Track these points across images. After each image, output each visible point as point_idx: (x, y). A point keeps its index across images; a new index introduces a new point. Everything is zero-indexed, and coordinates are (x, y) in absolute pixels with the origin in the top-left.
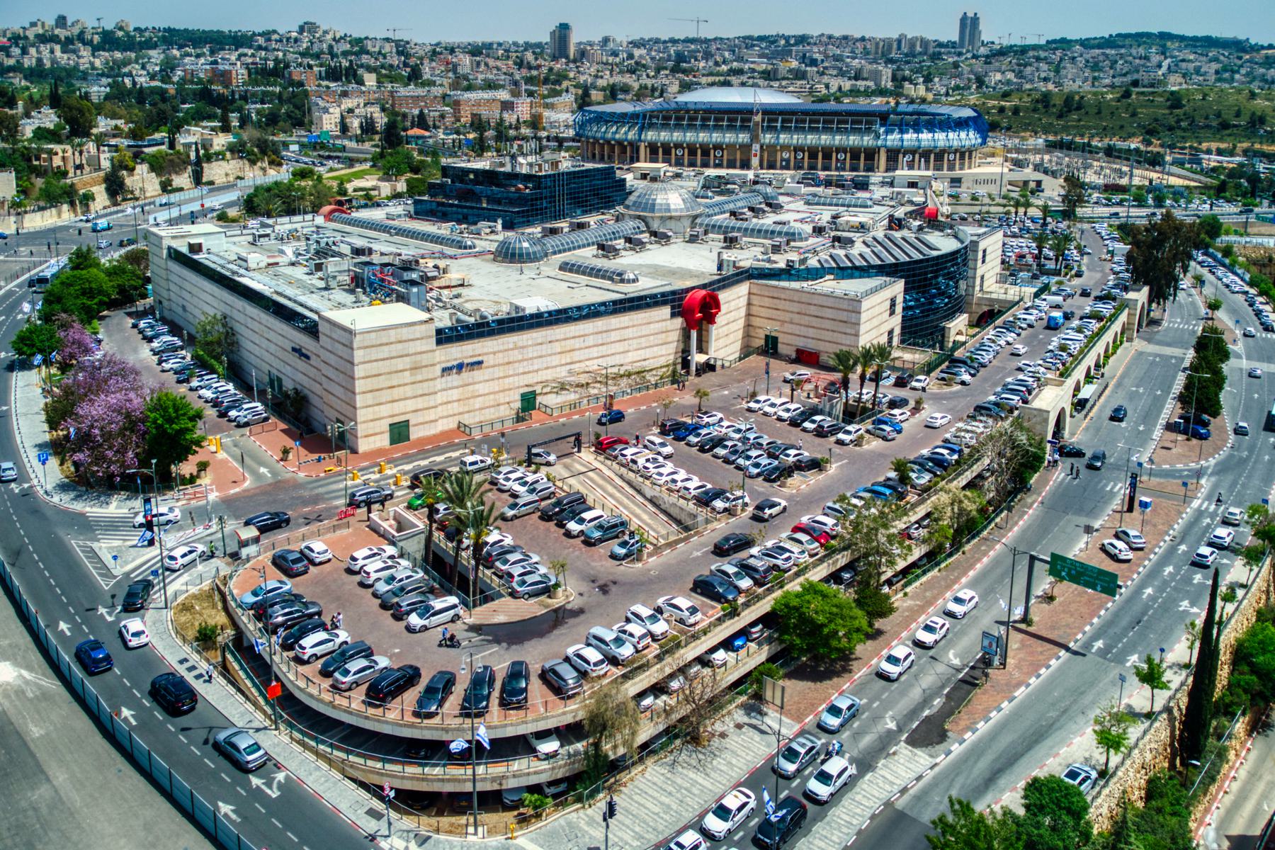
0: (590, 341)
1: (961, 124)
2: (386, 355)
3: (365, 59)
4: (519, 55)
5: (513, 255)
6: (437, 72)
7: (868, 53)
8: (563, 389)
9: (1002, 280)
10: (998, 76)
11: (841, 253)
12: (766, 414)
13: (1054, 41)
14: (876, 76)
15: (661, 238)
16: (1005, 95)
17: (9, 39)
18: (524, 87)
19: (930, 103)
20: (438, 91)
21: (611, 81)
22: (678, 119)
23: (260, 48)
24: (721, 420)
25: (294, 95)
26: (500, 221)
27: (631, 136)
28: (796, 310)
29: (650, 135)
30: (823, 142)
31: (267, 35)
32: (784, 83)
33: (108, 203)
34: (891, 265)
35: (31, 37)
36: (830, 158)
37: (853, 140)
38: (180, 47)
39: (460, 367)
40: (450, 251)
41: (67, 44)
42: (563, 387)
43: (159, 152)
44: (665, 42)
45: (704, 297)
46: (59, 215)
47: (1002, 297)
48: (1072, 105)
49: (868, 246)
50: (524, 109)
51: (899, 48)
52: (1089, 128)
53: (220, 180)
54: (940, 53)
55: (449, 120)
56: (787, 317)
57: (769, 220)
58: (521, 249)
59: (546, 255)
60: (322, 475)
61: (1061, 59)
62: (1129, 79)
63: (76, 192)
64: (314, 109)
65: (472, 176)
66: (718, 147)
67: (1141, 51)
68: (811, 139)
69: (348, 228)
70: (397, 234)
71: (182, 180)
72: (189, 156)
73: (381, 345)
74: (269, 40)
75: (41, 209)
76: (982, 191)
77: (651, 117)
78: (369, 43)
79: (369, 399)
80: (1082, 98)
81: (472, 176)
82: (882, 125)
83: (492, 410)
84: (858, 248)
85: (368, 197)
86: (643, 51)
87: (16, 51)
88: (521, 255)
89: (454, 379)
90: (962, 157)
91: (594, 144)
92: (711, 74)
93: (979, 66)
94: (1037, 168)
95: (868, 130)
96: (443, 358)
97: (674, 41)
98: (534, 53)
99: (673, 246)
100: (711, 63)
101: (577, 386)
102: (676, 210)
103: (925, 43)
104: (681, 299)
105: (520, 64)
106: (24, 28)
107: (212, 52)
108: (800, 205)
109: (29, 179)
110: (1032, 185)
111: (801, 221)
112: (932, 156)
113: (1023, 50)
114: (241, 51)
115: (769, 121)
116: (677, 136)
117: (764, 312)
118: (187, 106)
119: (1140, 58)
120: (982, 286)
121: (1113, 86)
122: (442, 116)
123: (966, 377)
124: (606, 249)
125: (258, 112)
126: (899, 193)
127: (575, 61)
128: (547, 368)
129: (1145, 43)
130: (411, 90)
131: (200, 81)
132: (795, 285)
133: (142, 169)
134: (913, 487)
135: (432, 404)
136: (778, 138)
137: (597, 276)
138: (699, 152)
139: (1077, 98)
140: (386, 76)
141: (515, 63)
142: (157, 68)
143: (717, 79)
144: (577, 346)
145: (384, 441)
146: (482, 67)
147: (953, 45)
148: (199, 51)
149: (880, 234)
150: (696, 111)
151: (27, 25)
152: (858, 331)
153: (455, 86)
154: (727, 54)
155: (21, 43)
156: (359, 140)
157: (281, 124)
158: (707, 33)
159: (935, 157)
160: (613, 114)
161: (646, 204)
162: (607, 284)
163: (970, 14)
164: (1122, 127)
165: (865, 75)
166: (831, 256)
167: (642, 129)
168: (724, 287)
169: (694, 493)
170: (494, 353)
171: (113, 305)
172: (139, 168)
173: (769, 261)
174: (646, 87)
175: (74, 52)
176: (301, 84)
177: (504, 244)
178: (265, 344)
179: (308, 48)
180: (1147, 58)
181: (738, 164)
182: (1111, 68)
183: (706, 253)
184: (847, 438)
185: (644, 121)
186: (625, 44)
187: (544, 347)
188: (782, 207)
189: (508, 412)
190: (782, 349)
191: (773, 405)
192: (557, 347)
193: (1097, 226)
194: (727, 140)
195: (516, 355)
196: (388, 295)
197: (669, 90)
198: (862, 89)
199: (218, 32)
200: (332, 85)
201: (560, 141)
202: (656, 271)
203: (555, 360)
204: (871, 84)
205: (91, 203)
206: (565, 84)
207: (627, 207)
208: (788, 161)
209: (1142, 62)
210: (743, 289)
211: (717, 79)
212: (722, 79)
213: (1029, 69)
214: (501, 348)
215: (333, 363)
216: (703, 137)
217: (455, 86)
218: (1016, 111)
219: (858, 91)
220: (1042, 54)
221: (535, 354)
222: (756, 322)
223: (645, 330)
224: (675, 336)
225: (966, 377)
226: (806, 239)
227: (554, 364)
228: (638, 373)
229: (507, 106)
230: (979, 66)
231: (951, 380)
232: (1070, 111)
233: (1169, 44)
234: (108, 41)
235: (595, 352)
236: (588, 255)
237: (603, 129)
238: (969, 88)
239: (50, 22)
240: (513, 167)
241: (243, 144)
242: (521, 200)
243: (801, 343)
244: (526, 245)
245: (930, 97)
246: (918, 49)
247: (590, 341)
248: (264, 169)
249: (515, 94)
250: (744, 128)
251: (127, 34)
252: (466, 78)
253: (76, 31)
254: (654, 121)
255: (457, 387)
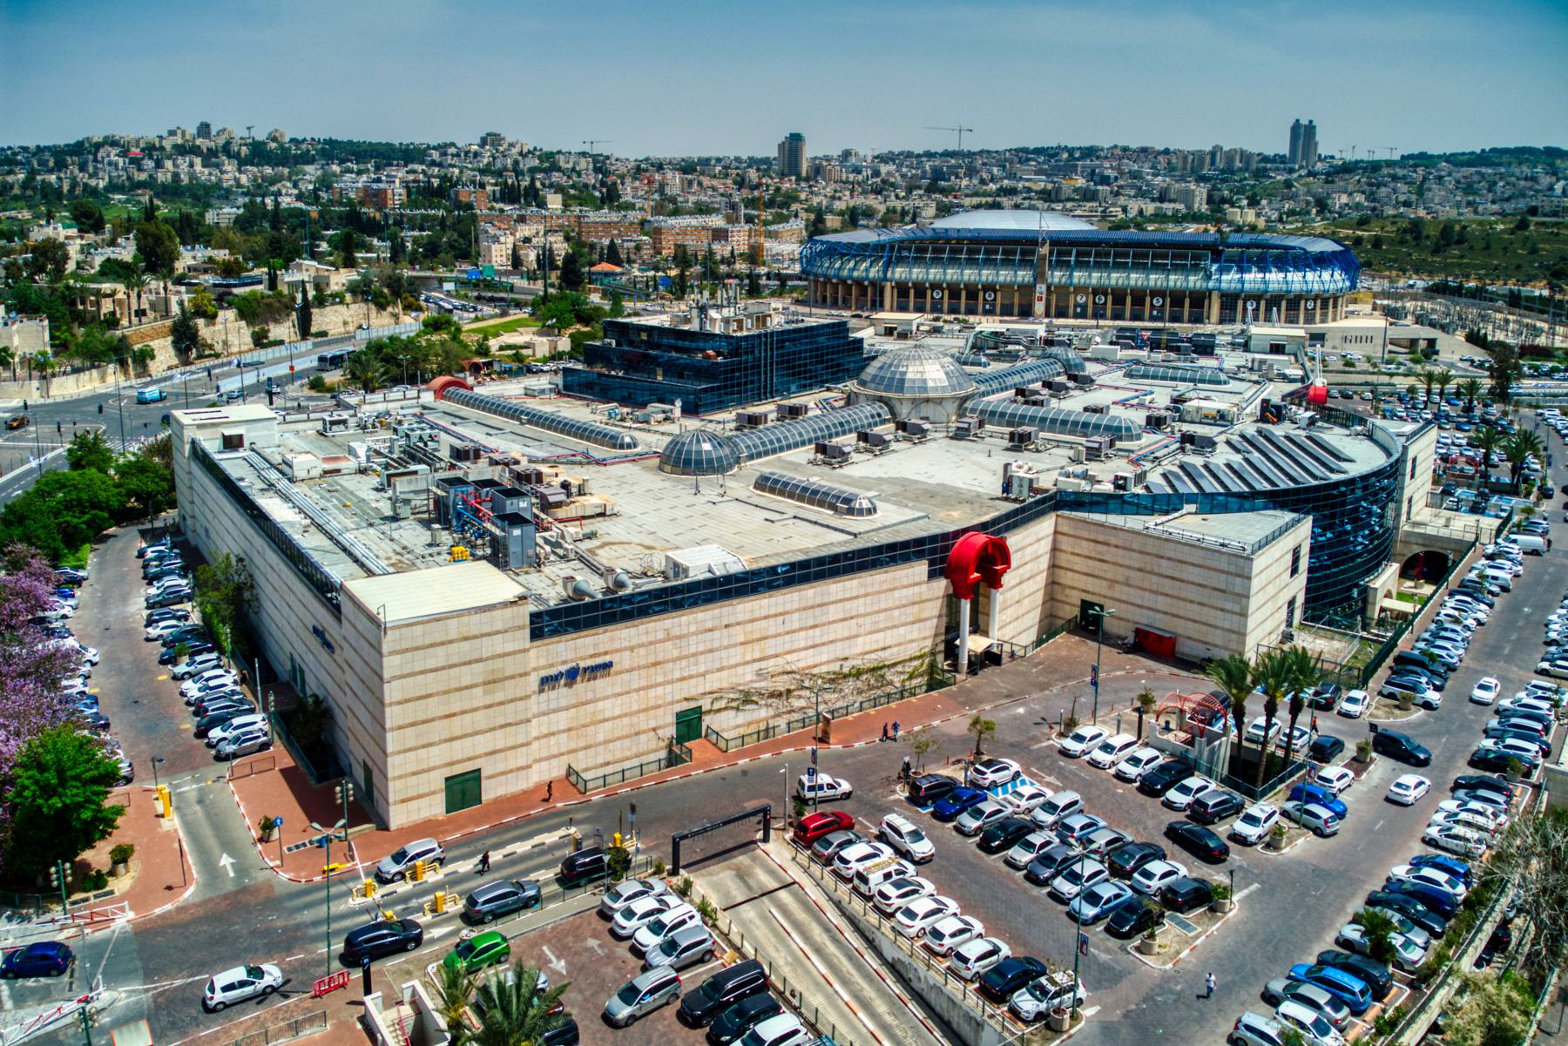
0: (795, 621)
1: (1320, 261)
2: (441, 663)
3: (556, 177)
4: (738, 172)
5: (687, 462)
6: (641, 193)
7: (1173, 169)
8: (747, 701)
9: (1435, 502)
10: (1344, 199)
11: (1197, 461)
12: (1094, 764)
13: (1411, 157)
14: (1187, 197)
15: (912, 432)
16: (1362, 223)
17: (143, 150)
18: (743, 211)
19: (1262, 232)
20: (634, 216)
21: (852, 203)
22: (935, 251)
23: (433, 163)
24: (1017, 774)
25: (459, 220)
26: (678, 403)
27: (873, 273)
28: (1136, 565)
29: (899, 273)
30: (1132, 283)
31: (442, 148)
32: (1069, 205)
33: (175, 361)
34: (1286, 492)
35: (168, 148)
36: (1143, 304)
37: (1175, 280)
38: (342, 162)
39: (572, 675)
40: (598, 451)
41: (210, 157)
42: (747, 698)
43: (253, 293)
44: (919, 156)
45: (985, 547)
46: (103, 379)
47: (1444, 533)
48: (1450, 236)
49: (1238, 451)
50: (740, 239)
51: (1213, 162)
52: (1476, 267)
53: (335, 330)
54: (1265, 170)
55: (646, 252)
56: (1120, 574)
57: (1074, 403)
58: (699, 452)
59: (738, 461)
60: (318, 879)
61: (1425, 179)
62: (1522, 204)
63: (128, 348)
64: (481, 237)
65: (644, 336)
66: (990, 287)
67: (1526, 170)
68: (1116, 278)
69: (465, 411)
70: (529, 422)
71: (282, 330)
72: (294, 299)
73: (432, 645)
74: (445, 154)
75: (76, 371)
76: (1356, 352)
77: (900, 249)
78: (562, 158)
79: (410, 737)
80: (1464, 227)
81: (644, 336)
82: (1214, 261)
83: (626, 742)
84: (1222, 456)
85: (518, 358)
86: (892, 167)
87: (149, 164)
88: (699, 462)
89: (562, 695)
90: (1324, 306)
91: (824, 284)
92: (976, 194)
93: (1318, 186)
94: (1419, 320)
95: (1195, 268)
96: (542, 662)
97: (930, 155)
98: (758, 170)
99: (931, 445)
100: (975, 181)
101: (772, 695)
102: (936, 389)
103: (1246, 157)
104: (946, 549)
105: (741, 183)
106: (161, 137)
107: (378, 168)
108: (1117, 377)
109: (69, 330)
110: (1422, 345)
111: (1123, 403)
112: (1284, 304)
113: (1375, 167)
114: (411, 167)
115: (1060, 254)
116: (934, 274)
117: (1079, 564)
118: (330, 232)
119: (1526, 179)
120: (1409, 513)
121: (1503, 214)
122: (638, 248)
123: (1432, 696)
124: (829, 454)
125: (415, 241)
126: (1262, 362)
127: (807, 179)
128: (721, 669)
129: (1527, 160)
130: (606, 215)
131: (350, 202)
132: (1135, 522)
133: (228, 315)
134: (1399, 965)
135: (521, 739)
136: (1071, 276)
137: (811, 502)
138: (964, 294)
139: (1457, 228)
140: (574, 197)
141: (735, 182)
142: (311, 187)
143: (984, 200)
144: (772, 631)
145: (435, 807)
146: (695, 187)
147: (1282, 159)
148: (362, 167)
149: (1251, 430)
150: (959, 241)
151: (165, 134)
152: (1247, 608)
153: (658, 210)
154: (995, 170)
155: (155, 154)
156: (532, 277)
157: (442, 255)
158: (971, 144)
159: (1291, 305)
160: (850, 246)
161: (892, 379)
162: (826, 515)
163: (1304, 122)
164: (1519, 267)
165: (1173, 196)
166: (1182, 467)
167: (887, 265)
168: (1015, 525)
169: (976, 967)
170: (632, 649)
171: (123, 517)
172: (221, 313)
173: (1085, 476)
174: (894, 211)
175: (217, 166)
176: (470, 206)
177: (676, 444)
178: (286, 610)
179: (489, 164)
180: (1533, 179)
181: (1016, 310)
182: (1489, 190)
183: (983, 459)
184: (1251, 832)
185: (892, 253)
186: (869, 159)
187: (717, 634)
188: (1092, 381)
189: (653, 745)
190: (1109, 625)
191: (1107, 748)
192: (739, 634)
193: (1547, 413)
194: (1001, 279)
195: (669, 650)
196: (480, 536)
197: (924, 214)
198: (1170, 213)
199: (388, 144)
200: (507, 208)
201: (783, 279)
202: (906, 491)
203: (736, 655)
204: (1181, 207)
205: (148, 361)
206: (794, 207)
207: (863, 383)
208: (1084, 307)
209: (1529, 184)
210: (1045, 526)
211: (984, 200)
212: (990, 200)
213: (1383, 191)
214: (644, 639)
215: (358, 669)
216: (969, 275)
217: (658, 210)
218: (1377, 243)
219: (1165, 215)
220: (1400, 172)
221: (701, 648)
222: (1066, 578)
223: (886, 601)
224: (935, 608)
225: (1432, 696)
226: (1139, 437)
227: (733, 661)
228: (873, 670)
229: (720, 235)
230: (1318, 186)
231: (1406, 699)
232: (1448, 245)
233: (1558, 162)
234: (258, 153)
235: (801, 639)
236: (798, 462)
237: (837, 265)
238: (1308, 213)
239: (192, 130)
240: (702, 323)
241: (366, 282)
242: (701, 372)
243: (1144, 619)
244: (707, 446)
245: (1261, 223)
246: (1238, 164)
247: (795, 621)
248: (396, 316)
249: (731, 220)
250: (1024, 263)
251: (281, 146)
252: (673, 200)
253: (221, 141)
254: (905, 254)
255: (567, 708)
